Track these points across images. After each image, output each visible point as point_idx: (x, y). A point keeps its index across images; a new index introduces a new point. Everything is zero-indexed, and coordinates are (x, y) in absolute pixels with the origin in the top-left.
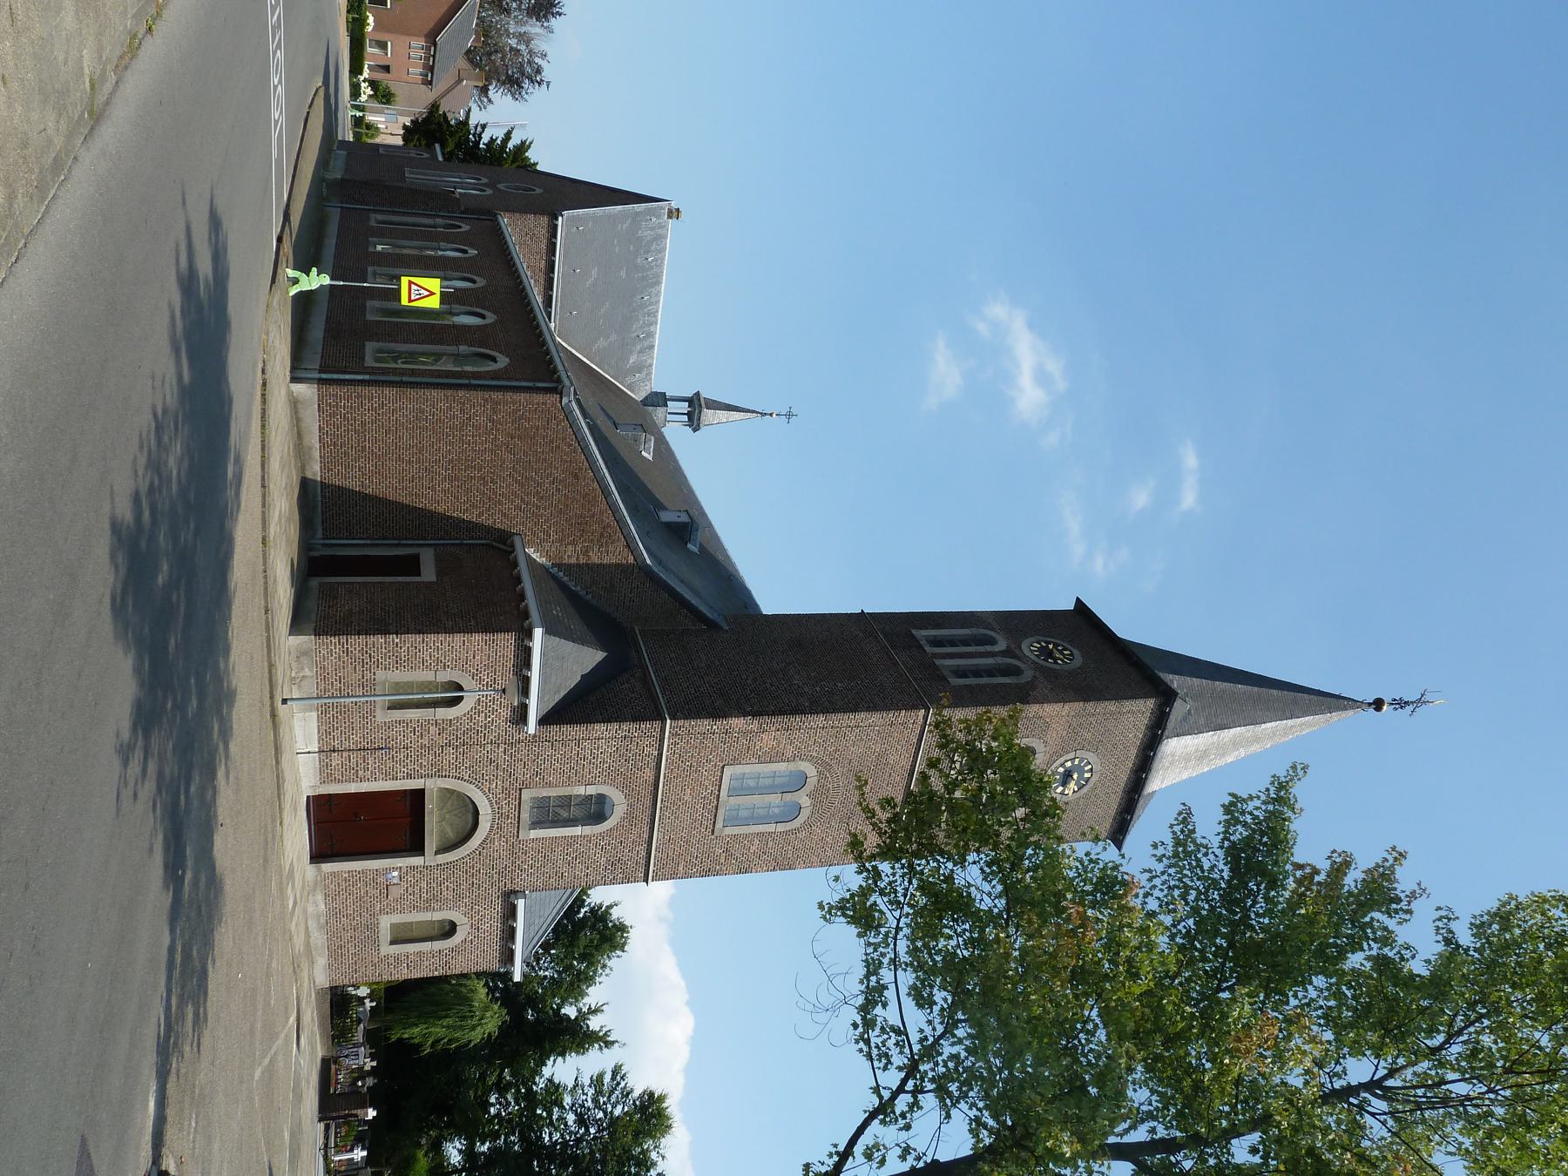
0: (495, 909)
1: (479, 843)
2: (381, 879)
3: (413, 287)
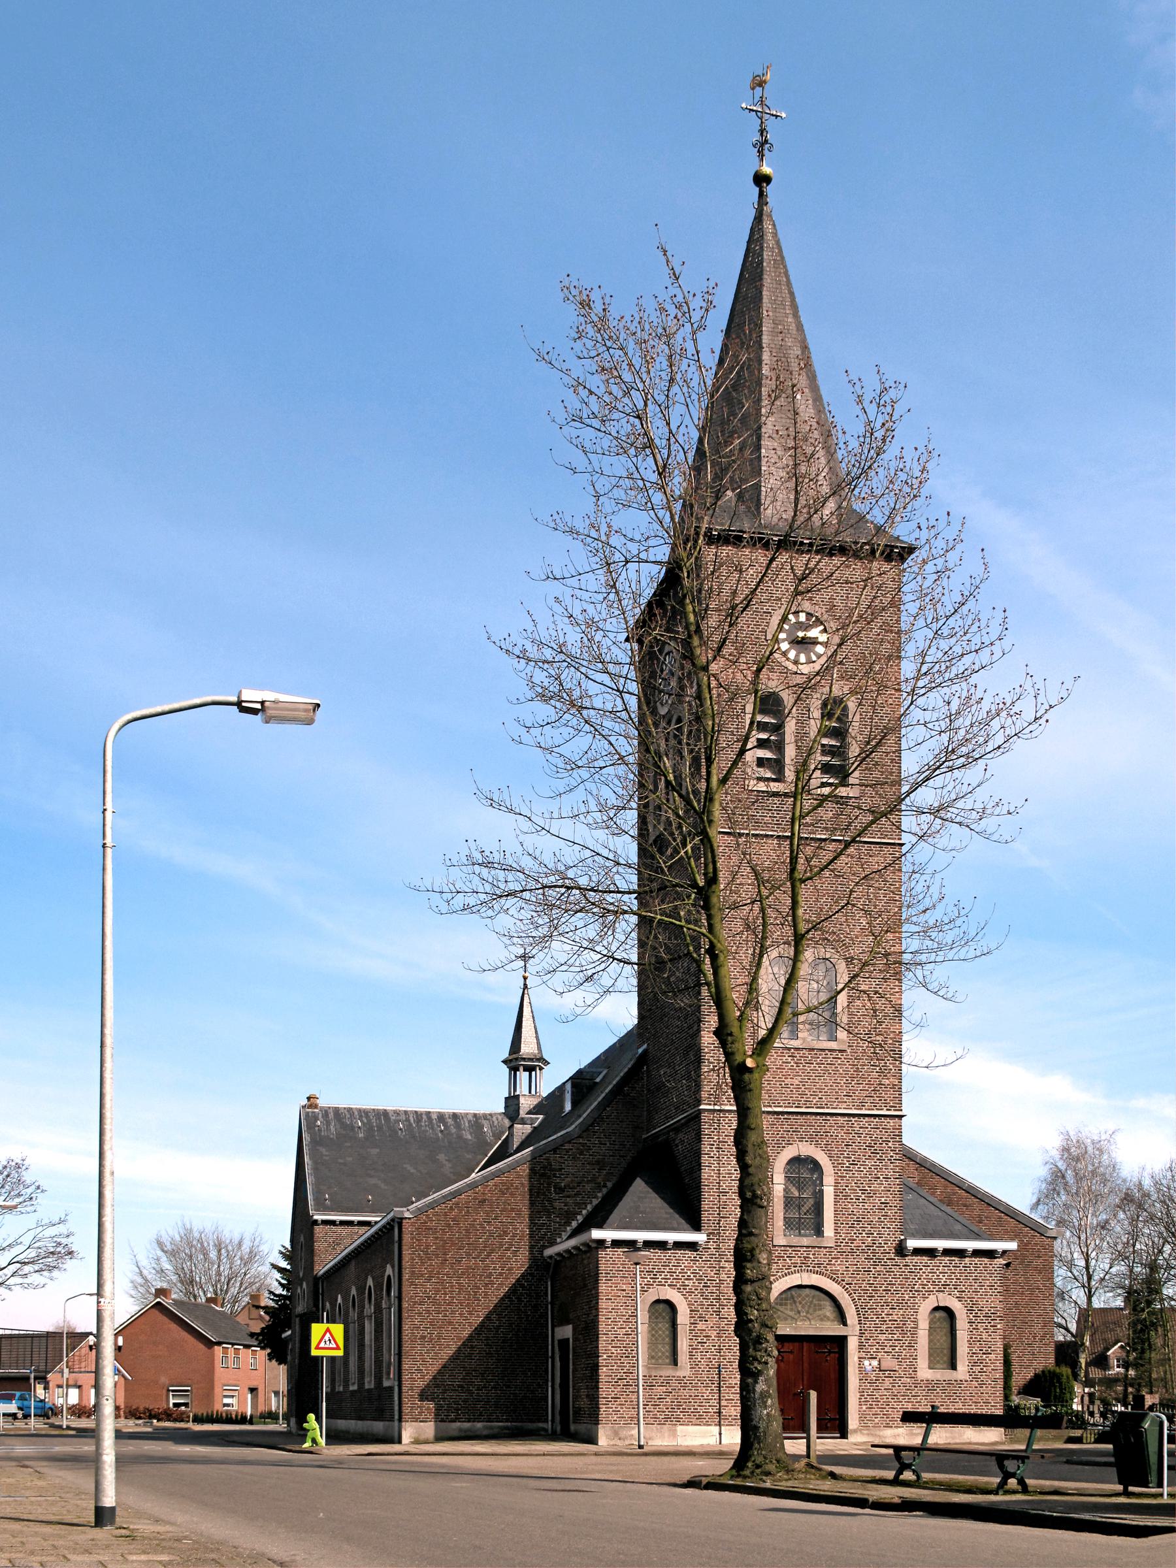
1: (836, 1284)
3: (322, 1345)
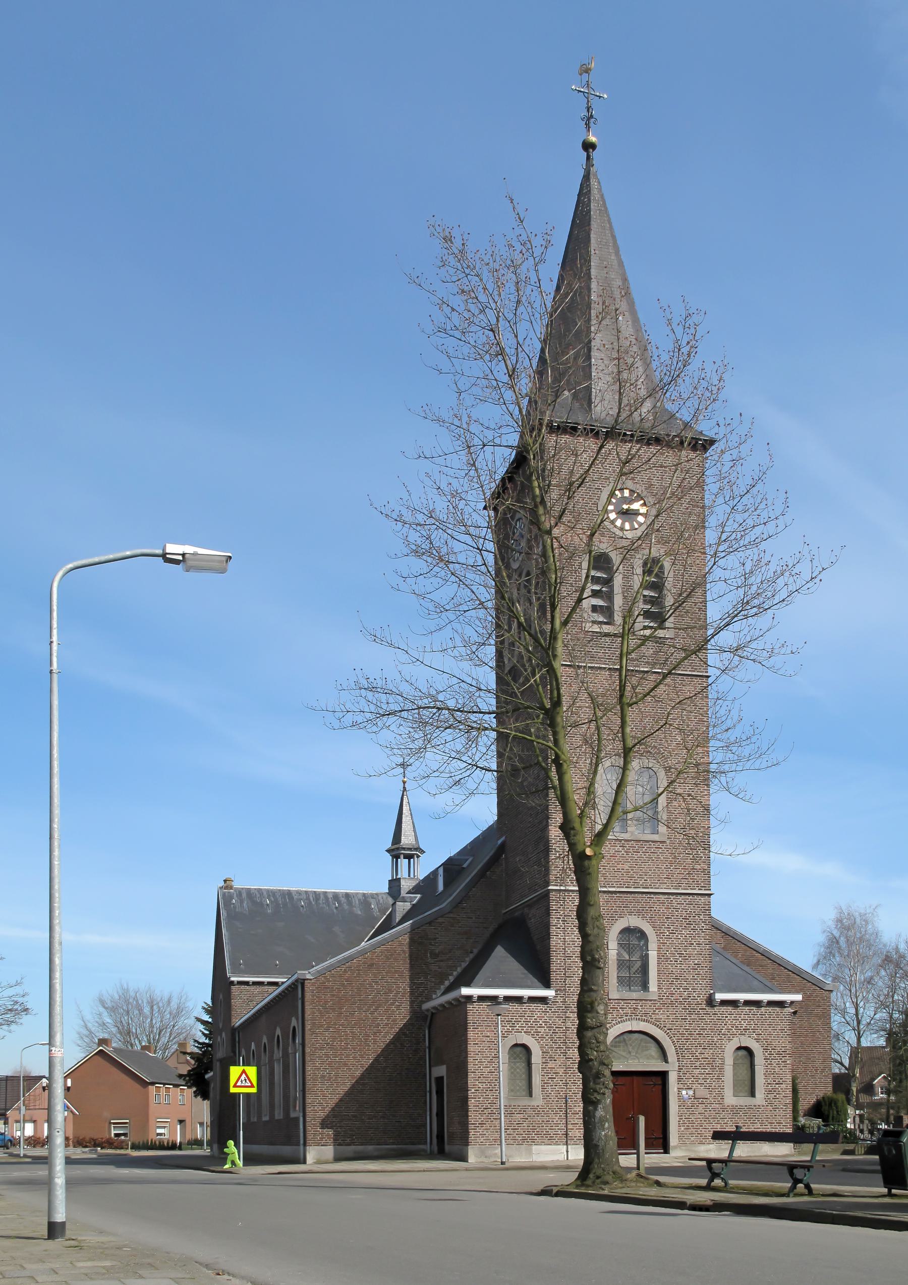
0: (727, 1017)
2: (689, 1103)
3: (239, 1084)
